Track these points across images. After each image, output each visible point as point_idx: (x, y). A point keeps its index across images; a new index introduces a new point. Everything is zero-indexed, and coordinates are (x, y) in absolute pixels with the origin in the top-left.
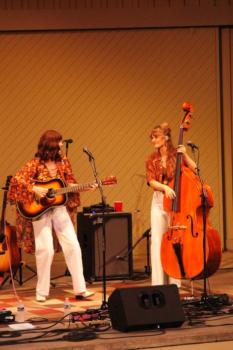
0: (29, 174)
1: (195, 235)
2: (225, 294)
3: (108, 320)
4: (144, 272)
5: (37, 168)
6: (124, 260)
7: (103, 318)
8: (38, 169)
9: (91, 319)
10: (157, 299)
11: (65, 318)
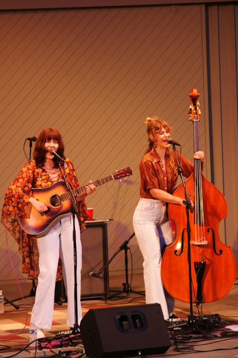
0: (26, 179)
1: (218, 252)
2: (216, 315)
3: (80, 347)
4: (122, 290)
5: (34, 171)
6: (98, 277)
7: (74, 345)
8: (35, 173)
9: (61, 346)
10: (137, 320)
11: (31, 345)
